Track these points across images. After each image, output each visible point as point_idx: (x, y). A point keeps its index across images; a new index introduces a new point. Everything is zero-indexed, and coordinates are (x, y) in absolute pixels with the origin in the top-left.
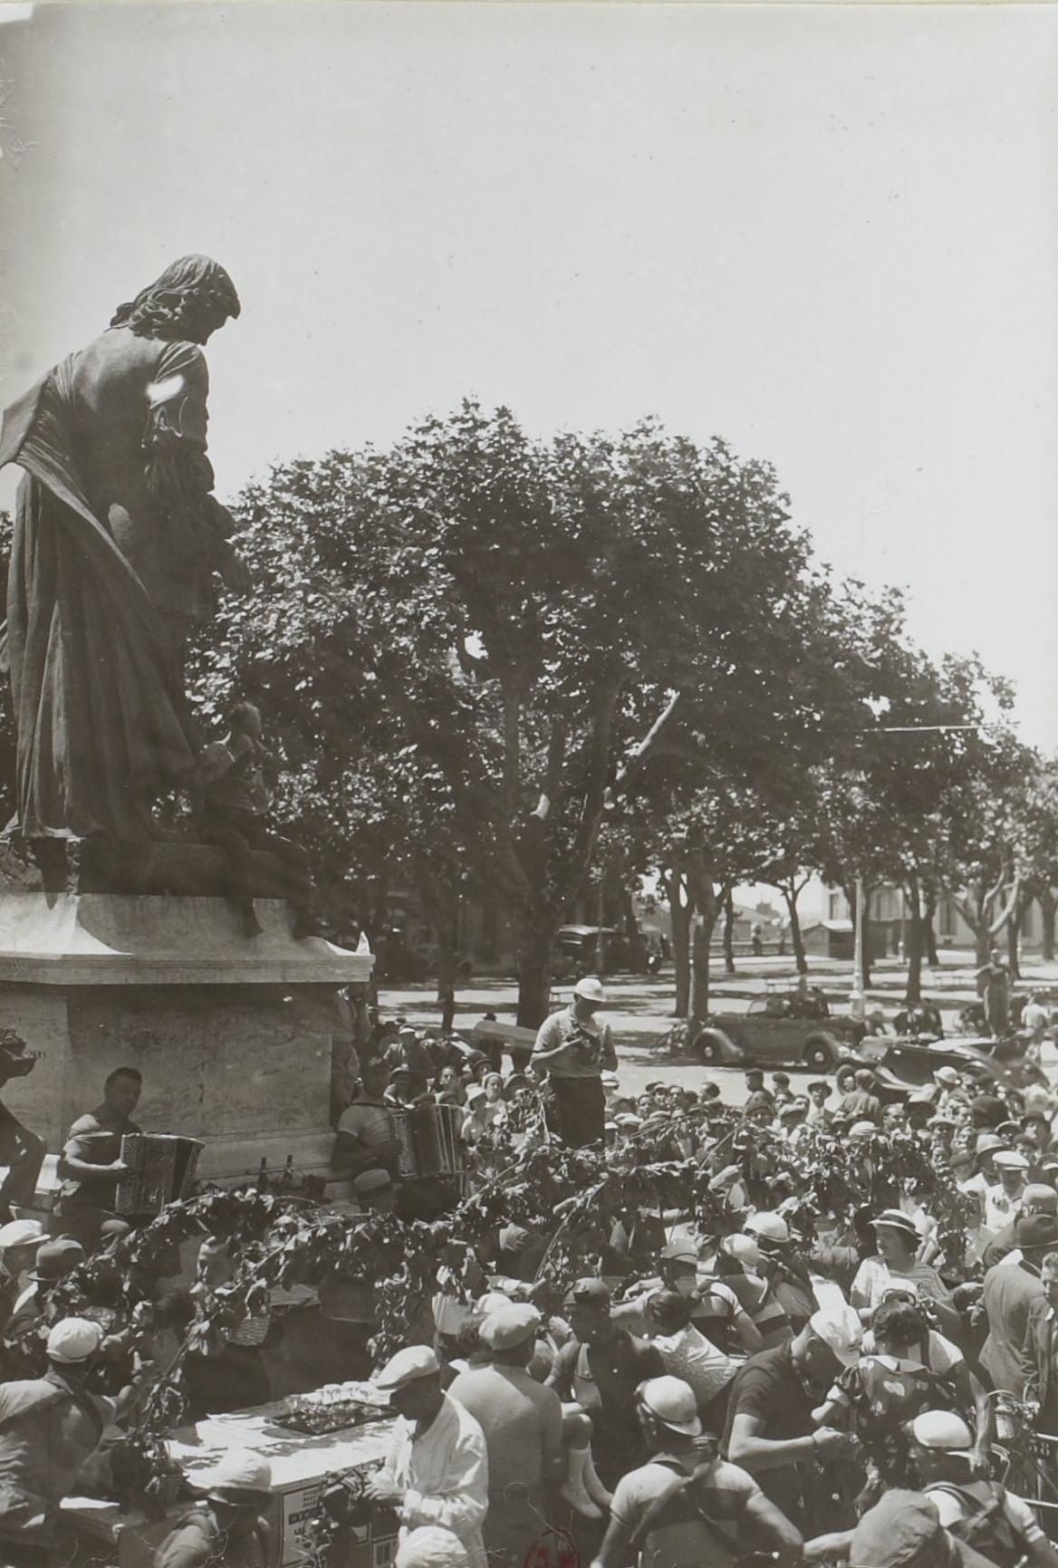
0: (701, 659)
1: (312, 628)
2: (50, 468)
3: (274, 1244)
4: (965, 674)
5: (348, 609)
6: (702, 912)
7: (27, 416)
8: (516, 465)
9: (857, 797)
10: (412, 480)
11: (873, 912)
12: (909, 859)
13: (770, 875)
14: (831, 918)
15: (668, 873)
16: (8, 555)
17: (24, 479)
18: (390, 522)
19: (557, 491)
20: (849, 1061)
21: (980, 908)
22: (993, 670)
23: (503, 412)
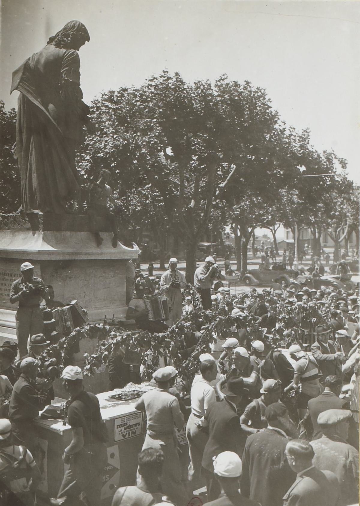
0: (243, 155)
1: (116, 146)
2: (28, 92)
3: (110, 341)
4: (330, 157)
5: (127, 140)
6: (245, 237)
7: (20, 74)
8: (182, 91)
9: (295, 199)
10: (148, 97)
11: (301, 237)
12: (312, 218)
13: (267, 224)
14: (287, 239)
15: (234, 225)
16: (15, 122)
17: (20, 96)
18: (140, 111)
19: (195, 100)
20: (293, 283)
21: (336, 235)
22: (339, 156)
23: (177, 74)
